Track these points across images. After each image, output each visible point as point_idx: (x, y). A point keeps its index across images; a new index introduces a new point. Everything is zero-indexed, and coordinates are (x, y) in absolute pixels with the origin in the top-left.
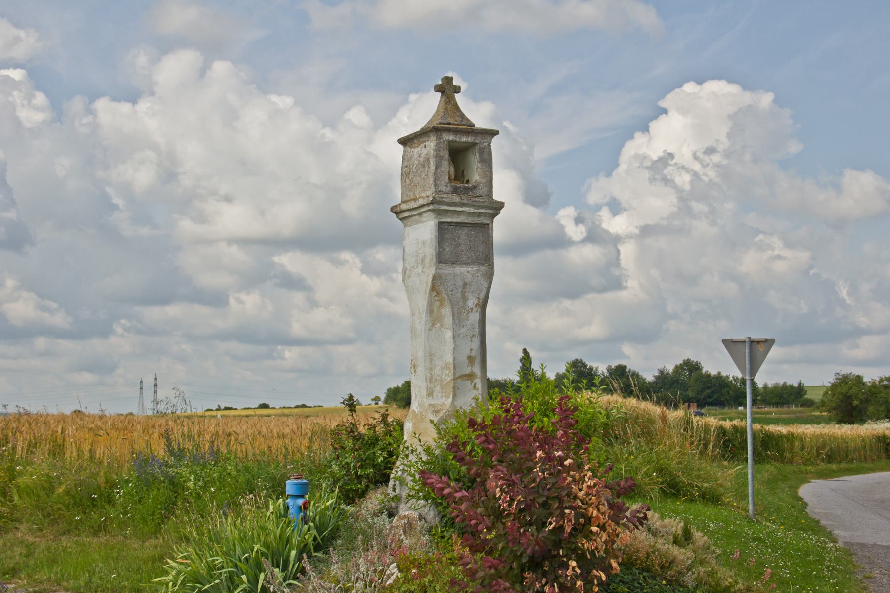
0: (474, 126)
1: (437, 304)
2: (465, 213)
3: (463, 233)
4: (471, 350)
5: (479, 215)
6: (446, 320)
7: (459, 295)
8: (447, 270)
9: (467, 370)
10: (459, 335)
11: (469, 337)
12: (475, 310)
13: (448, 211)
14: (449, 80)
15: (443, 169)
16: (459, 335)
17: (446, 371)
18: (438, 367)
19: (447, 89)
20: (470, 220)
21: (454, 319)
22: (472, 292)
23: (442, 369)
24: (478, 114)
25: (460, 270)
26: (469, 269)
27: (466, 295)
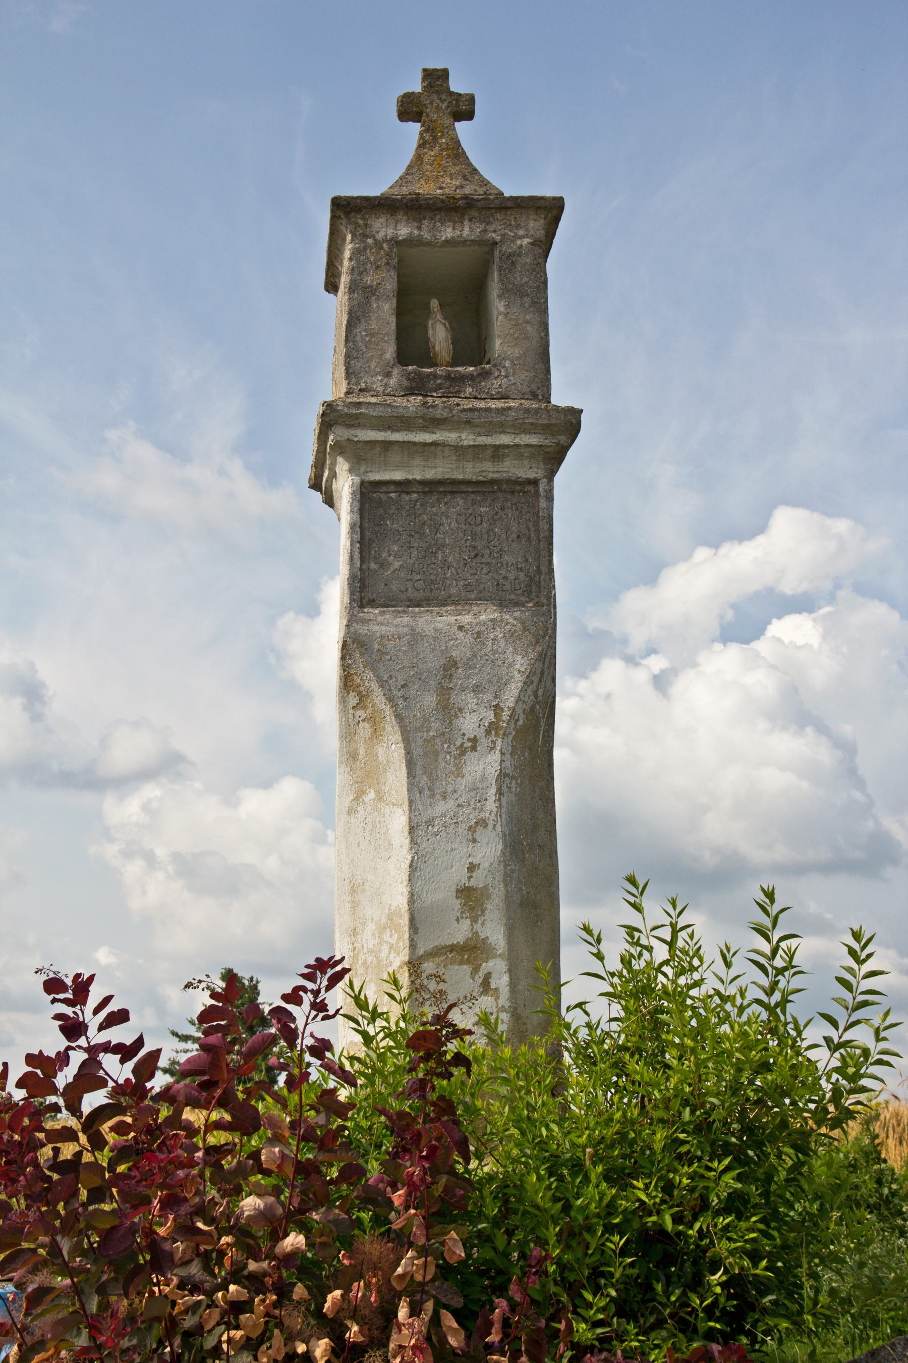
0: (503, 194)
1: (365, 730)
2: (446, 451)
3: (451, 514)
4: (472, 868)
5: (497, 453)
6: (391, 777)
7: (430, 700)
8: (384, 623)
9: (460, 932)
10: (430, 822)
11: (462, 829)
12: (484, 742)
13: (387, 445)
14: (436, 79)
15: (374, 325)
16: (430, 822)
17: (391, 938)
18: (371, 927)
19: (436, 105)
20: (469, 471)
21: (411, 774)
22: (477, 689)
23: (382, 929)
24: (501, 157)
25: (440, 622)
26: (466, 619)
27: (457, 699)
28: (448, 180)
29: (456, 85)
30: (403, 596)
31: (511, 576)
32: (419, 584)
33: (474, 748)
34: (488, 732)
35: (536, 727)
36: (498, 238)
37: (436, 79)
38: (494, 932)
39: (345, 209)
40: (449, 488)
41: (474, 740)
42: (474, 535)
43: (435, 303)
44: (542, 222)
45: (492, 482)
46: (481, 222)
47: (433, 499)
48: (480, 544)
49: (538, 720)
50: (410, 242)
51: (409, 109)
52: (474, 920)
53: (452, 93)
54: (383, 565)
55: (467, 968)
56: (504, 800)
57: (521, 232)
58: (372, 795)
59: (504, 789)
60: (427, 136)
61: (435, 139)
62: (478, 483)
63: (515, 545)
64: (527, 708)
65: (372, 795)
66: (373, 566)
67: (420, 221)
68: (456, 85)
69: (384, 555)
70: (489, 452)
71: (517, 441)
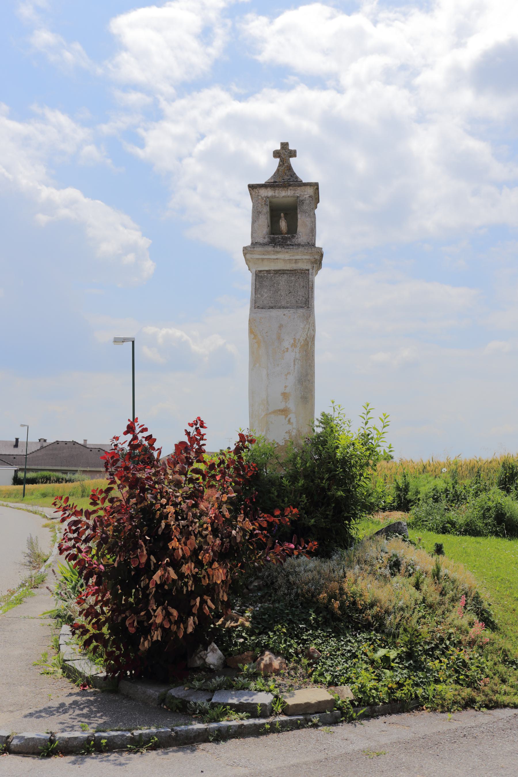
0: (302, 181)
3: (283, 280)
4: (286, 387)
5: (296, 261)
9: (282, 406)
13: (263, 259)
14: (284, 145)
28: (286, 177)
29: (291, 147)
30: (268, 305)
31: (301, 299)
32: (273, 302)
33: (287, 351)
34: (292, 346)
35: (307, 345)
36: (299, 195)
37: (284, 145)
38: (291, 405)
39: (252, 187)
40: (282, 272)
41: (287, 349)
42: (289, 286)
43: (282, 215)
44: (312, 190)
45: (295, 270)
46: (293, 190)
47: (277, 275)
48: (291, 289)
49: (308, 342)
50: (273, 197)
51: (276, 154)
52: (286, 402)
53: (289, 150)
54: (262, 296)
55: (284, 417)
56: (296, 367)
57: (306, 193)
58: (258, 365)
59: (296, 363)
60: (281, 163)
61: (284, 164)
62: (291, 270)
63: (302, 289)
64: (304, 339)
65: (258, 365)
66: (259, 296)
67: (275, 190)
68: (291, 147)
69: (262, 292)
70: (294, 261)
71: (302, 258)
